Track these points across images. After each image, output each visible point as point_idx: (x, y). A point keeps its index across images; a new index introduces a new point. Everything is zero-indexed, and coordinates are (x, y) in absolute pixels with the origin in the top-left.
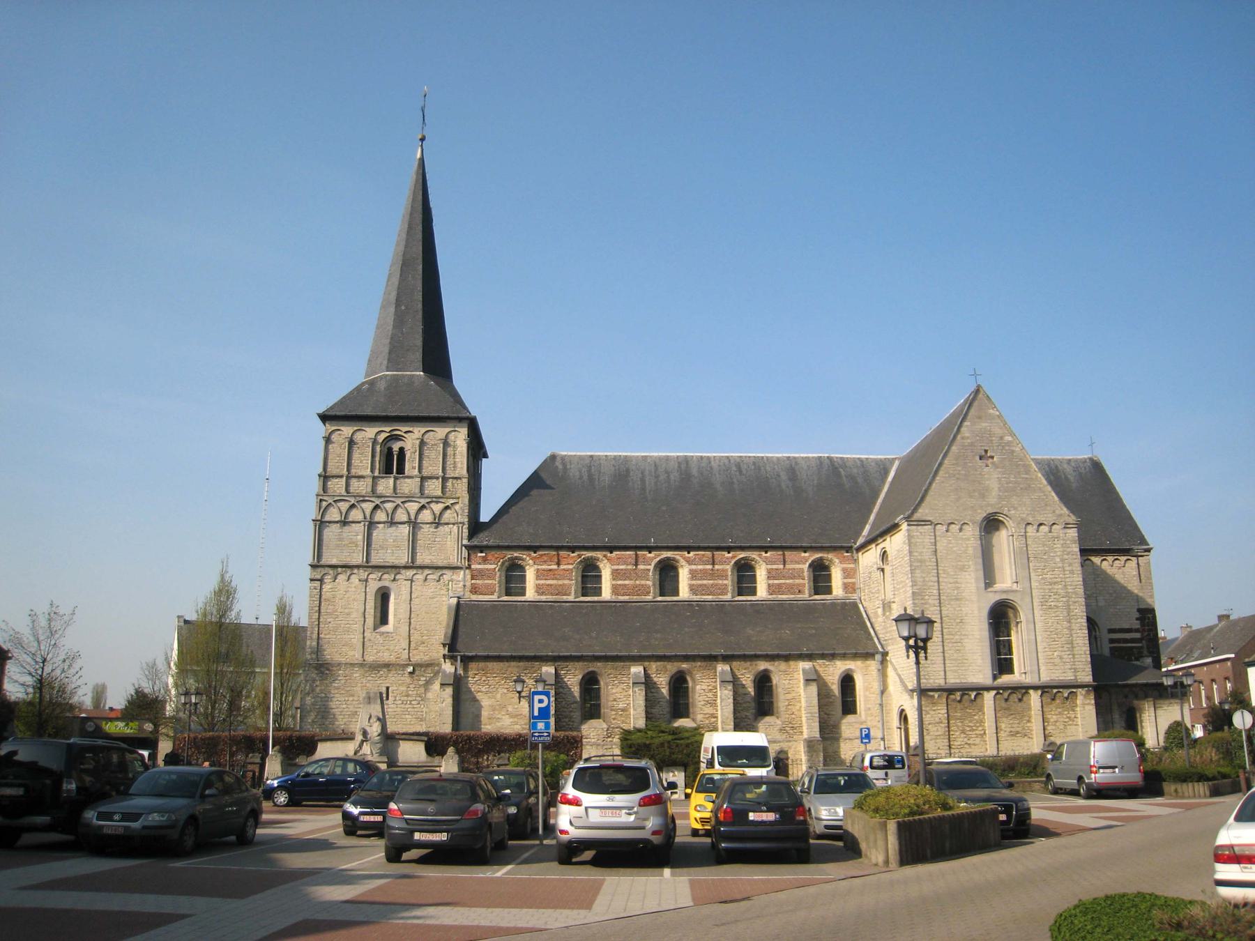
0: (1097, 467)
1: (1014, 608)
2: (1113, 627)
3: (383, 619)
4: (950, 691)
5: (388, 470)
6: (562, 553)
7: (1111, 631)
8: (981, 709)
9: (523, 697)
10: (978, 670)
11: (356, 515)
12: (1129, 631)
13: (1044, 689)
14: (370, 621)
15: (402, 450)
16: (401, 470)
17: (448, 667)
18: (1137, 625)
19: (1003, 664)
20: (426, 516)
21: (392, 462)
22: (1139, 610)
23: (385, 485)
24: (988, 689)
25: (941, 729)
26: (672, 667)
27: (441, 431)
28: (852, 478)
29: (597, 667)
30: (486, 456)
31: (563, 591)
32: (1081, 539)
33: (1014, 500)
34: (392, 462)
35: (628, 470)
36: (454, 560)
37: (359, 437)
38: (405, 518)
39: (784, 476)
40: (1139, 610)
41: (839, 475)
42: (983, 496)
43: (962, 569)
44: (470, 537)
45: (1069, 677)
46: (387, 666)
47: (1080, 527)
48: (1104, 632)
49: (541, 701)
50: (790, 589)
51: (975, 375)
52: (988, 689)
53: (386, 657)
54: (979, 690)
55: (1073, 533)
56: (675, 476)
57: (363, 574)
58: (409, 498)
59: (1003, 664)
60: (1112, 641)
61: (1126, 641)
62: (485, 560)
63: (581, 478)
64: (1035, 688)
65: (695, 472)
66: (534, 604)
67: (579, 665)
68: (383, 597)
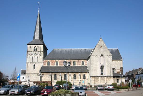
0: (118, 50)
1: (104, 67)
3: (35, 68)
4: (95, 77)
5: (35, 51)
6: (54, 60)
7: (117, 70)
8: (99, 79)
10: (99, 74)
11: (31, 56)
12: (119, 70)
13: (107, 76)
14: (33, 69)
15: (36, 48)
16: (36, 51)
17: (40, 74)
18: (120, 69)
19: (102, 74)
20: (39, 56)
21: (35, 50)
22: (121, 67)
23: (34, 52)
24: (100, 76)
25: (94, 81)
26: (64, 74)
27: (40, 46)
28: (88, 51)
29: (56, 73)
30: (48, 50)
31: (54, 65)
32: (113, 58)
33: (105, 53)
34: (35, 50)
35: (62, 51)
36: (42, 62)
37: (31, 47)
38: (36, 56)
39: (80, 51)
40: (121, 67)
41: (86, 51)
42: (101, 52)
43: (97, 61)
44: (44, 59)
45: (110, 75)
46: (35, 74)
47: (113, 56)
48: (116, 70)
49: (18, 75)
50: (79, 65)
52: (100, 76)
53: (35, 73)
54: (99, 77)
55: (112, 57)
56: (67, 51)
57: (32, 63)
58: (37, 54)
59: (102, 74)
60: (117, 71)
61: (119, 71)
62: (45, 61)
63: (64, 53)
64: (105, 76)
65: (70, 51)
66: (51, 67)
67: (54, 73)
68: (34, 65)
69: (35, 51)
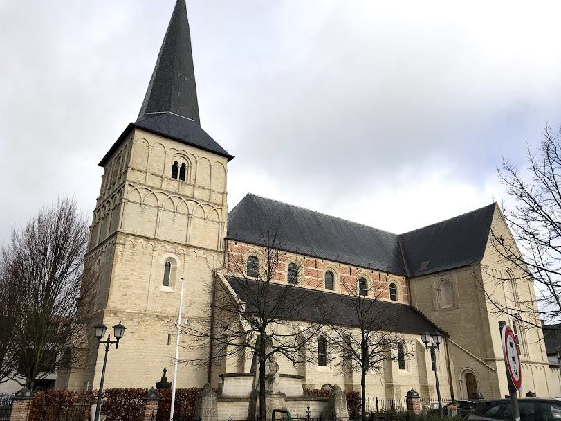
2: (162, 279)
9: (102, 342)
51: (493, 198)
69: (174, 175)
